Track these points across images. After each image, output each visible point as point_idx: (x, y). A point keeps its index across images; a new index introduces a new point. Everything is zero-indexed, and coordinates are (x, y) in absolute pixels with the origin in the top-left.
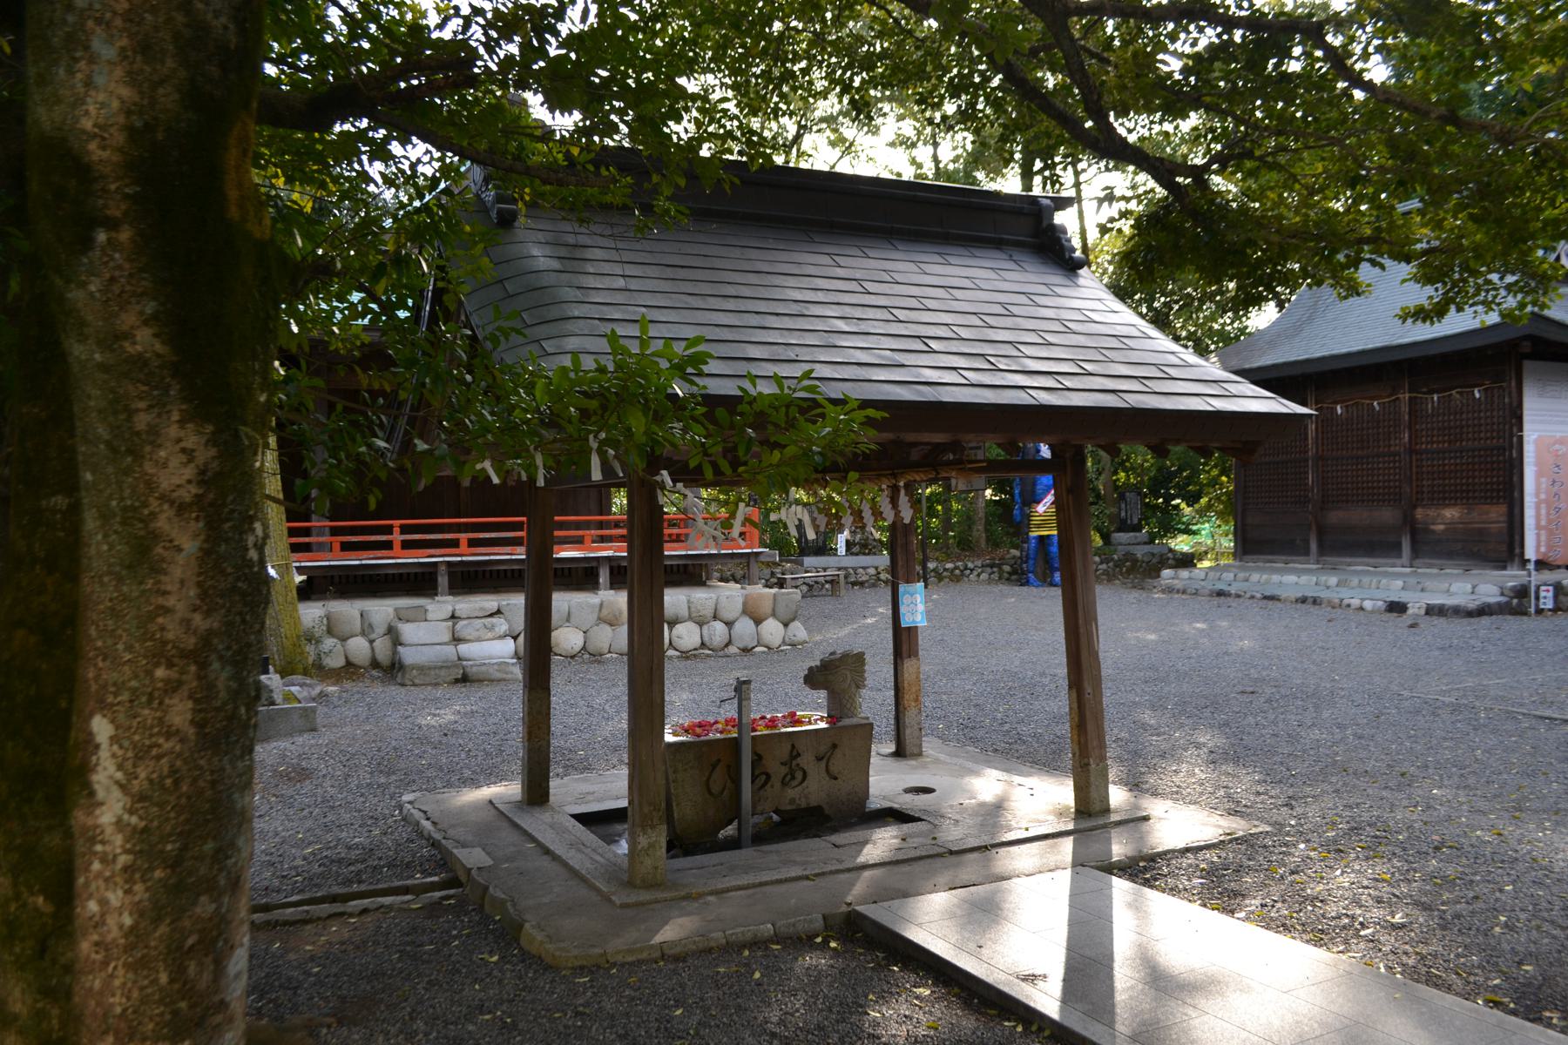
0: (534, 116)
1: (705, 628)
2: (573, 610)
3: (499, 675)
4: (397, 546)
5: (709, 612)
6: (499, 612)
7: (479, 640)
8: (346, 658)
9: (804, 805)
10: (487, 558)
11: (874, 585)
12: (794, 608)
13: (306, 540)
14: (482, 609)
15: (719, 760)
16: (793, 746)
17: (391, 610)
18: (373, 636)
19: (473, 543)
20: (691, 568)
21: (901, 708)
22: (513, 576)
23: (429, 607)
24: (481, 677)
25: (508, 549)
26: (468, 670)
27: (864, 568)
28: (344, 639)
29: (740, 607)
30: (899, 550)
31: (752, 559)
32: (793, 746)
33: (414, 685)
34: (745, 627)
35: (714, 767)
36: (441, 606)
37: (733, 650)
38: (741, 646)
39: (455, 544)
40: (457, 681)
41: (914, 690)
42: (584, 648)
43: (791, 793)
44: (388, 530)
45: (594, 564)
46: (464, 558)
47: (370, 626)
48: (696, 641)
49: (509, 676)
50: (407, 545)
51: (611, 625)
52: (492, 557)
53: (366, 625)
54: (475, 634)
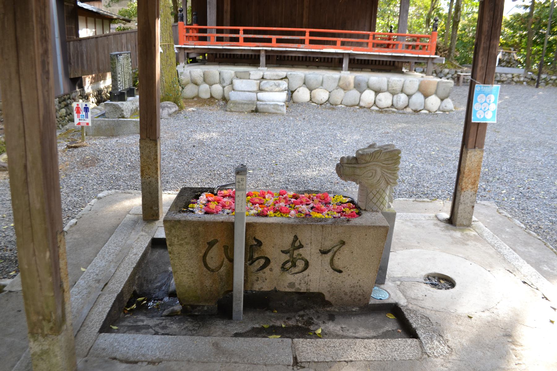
1: (395, 96)
2: (324, 80)
3: (274, 111)
4: (241, 40)
5: (399, 88)
6: (286, 77)
7: (271, 91)
8: (211, 94)
9: (303, 289)
10: (284, 49)
11: (509, 83)
12: (448, 91)
13: (205, 35)
14: (277, 75)
15: (215, 241)
16: (296, 238)
17: (233, 72)
18: (224, 85)
20: (396, 64)
21: (459, 188)
22: (230, 57)
23: (251, 73)
24: (265, 111)
25: (296, 45)
26: (258, 106)
27: (506, 74)
28: (211, 85)
29: (416, 87)
30: (481, 53)
31: (430, 61)
32: (296, 238)
33: (231, 111)
34: (418, 98)
35: (211, 244)
36: (256, 73)
37: (409, 110)
38: (414, 108)
39: (269, 41)
40: (252, 111)
41: (473, 175)
42: (328, 100)
43: (289, 278)
44: (303, 34)
45: (341, 57)
46: (273, 49)
47: (223, 79)
48: (389, 103)
49: (279, 112)
50: (246, 40)
51: (344, 90)
53: (222, 78)
54: (270, 88)
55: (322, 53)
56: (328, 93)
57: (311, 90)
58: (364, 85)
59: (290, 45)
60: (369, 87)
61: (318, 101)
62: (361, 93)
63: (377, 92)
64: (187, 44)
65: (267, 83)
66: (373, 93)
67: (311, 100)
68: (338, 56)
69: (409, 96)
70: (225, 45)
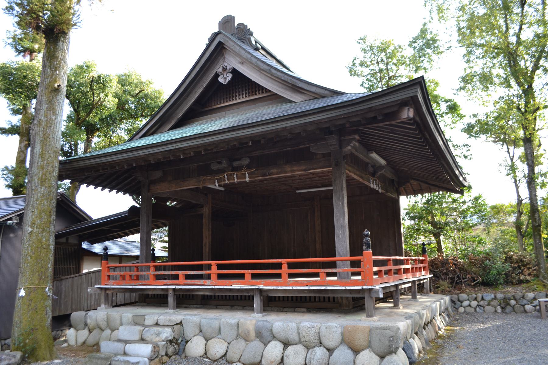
0: (14, 165)
4: (214, 277)
12: (387, 343)
14: (170, 320)
19: (188, 277)
39: (176, 277)
42: (225, 355)
44: (209, 267)
45: (251, 294)
48: (222, 352)
50: (220, 277)
51: (246, 341)
52: (201, 287)
55: (231, 290)
56: (226, 344)
57: (207, 340)
58: (265, 333)
59: (196, 282)
60: (274, 337)
61: (212, 355)
62: (266, 345)
63: (286, 344)
64: (107, 283)
65: (148, 330)
66: (280, 346)
67: (206, 354)
68: (248, 293)
69: (330, 351)
70: (138, 284)
